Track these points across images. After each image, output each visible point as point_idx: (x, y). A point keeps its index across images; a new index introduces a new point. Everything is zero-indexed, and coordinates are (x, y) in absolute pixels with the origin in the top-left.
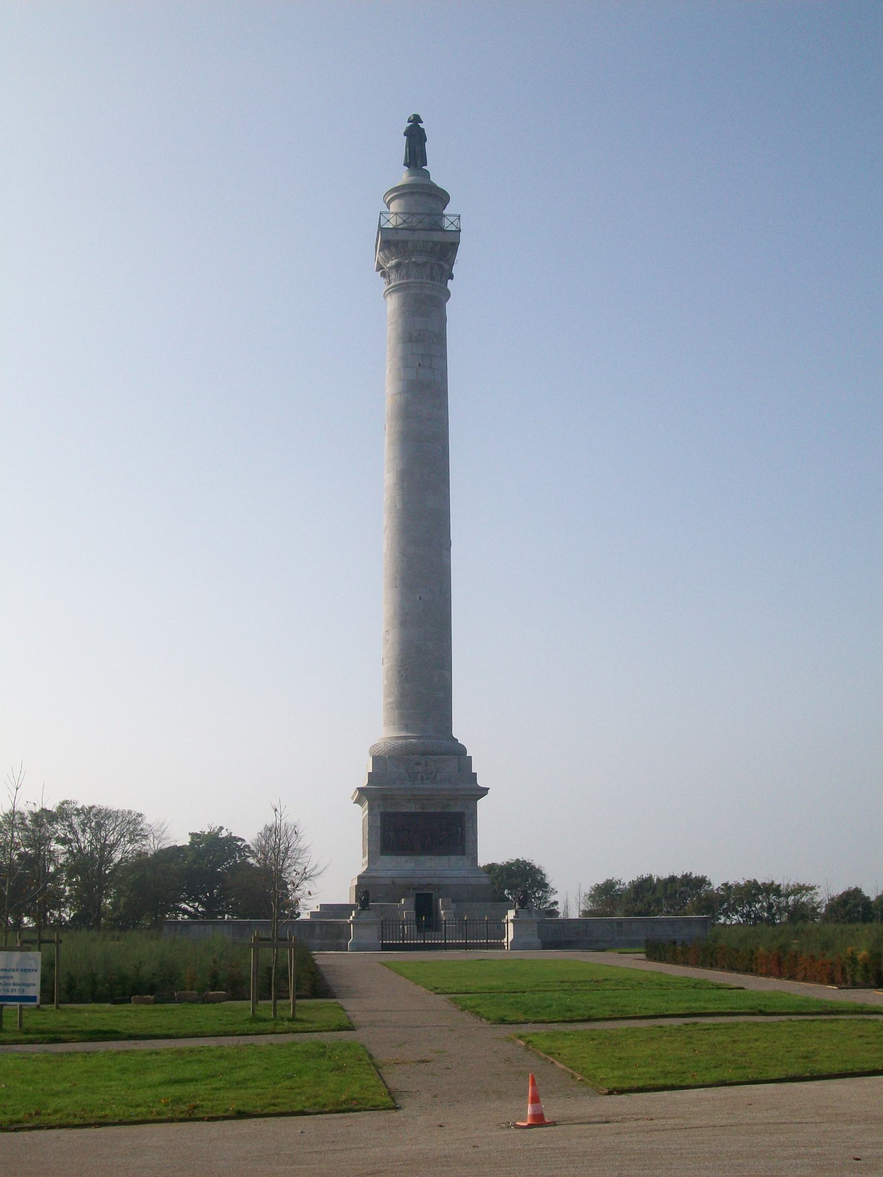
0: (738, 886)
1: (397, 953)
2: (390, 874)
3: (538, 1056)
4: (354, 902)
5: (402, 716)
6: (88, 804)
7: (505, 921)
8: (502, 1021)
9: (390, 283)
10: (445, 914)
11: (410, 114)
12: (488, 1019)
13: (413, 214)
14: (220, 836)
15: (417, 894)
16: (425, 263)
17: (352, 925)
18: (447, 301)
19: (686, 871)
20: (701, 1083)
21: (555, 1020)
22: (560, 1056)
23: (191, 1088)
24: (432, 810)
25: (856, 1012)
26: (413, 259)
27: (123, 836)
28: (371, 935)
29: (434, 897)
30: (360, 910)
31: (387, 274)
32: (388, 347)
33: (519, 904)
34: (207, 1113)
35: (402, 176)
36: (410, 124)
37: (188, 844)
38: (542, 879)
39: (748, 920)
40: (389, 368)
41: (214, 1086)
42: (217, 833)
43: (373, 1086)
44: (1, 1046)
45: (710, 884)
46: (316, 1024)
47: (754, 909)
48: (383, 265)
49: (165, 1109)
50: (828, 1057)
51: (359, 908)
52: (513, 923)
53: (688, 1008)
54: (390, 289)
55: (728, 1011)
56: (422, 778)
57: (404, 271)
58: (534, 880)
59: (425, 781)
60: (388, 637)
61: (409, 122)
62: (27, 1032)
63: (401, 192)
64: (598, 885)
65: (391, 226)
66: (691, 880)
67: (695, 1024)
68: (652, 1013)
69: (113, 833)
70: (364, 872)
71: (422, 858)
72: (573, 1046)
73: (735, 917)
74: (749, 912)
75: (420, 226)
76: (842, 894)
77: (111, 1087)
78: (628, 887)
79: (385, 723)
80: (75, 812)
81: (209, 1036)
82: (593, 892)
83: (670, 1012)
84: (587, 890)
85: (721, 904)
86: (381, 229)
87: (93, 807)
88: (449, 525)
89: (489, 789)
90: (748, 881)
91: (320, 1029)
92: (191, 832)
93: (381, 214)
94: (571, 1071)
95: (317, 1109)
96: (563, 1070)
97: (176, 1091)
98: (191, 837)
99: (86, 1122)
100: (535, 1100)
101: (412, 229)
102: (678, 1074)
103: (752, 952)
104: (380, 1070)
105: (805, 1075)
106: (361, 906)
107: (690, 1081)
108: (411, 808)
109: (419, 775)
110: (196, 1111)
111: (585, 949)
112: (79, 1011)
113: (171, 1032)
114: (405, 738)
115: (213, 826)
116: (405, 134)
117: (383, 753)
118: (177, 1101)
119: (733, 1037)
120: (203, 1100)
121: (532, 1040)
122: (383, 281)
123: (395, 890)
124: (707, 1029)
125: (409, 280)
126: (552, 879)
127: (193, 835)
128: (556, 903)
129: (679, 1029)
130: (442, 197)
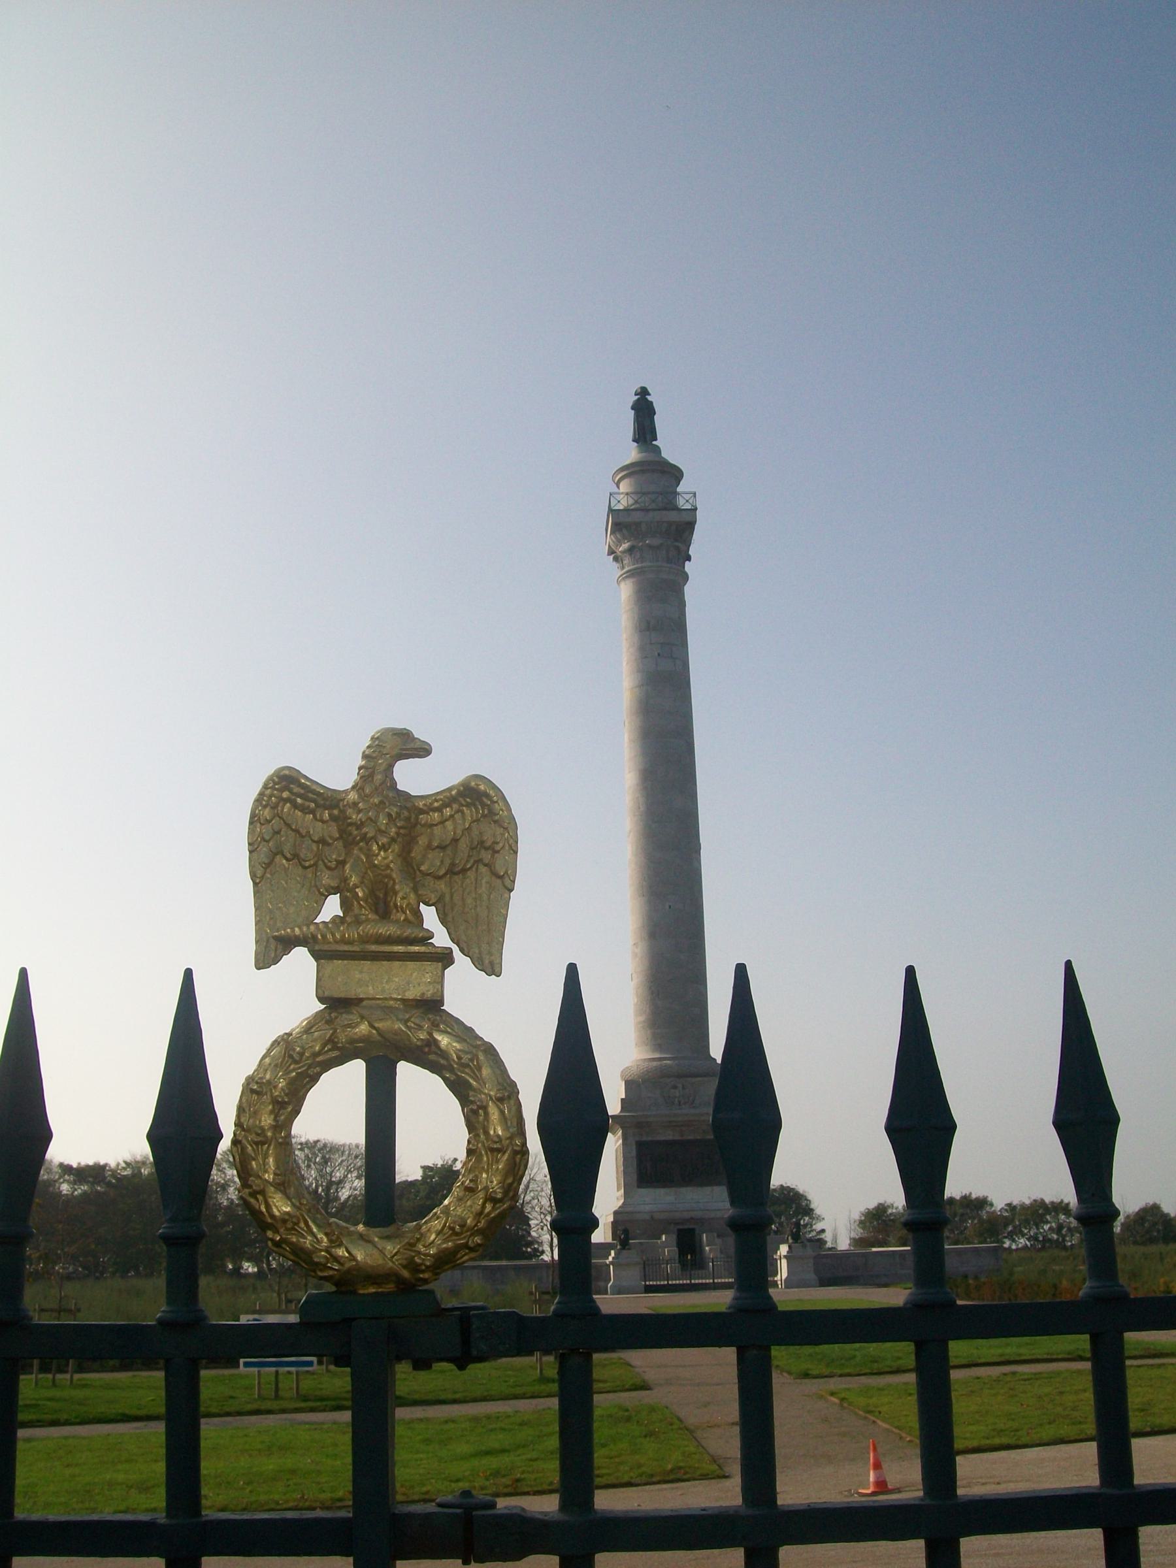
0: (1023, 1207)
1: (663, 1296)
2: (648, 1208)
3: (856, 1414)
4: (609, 1240)
5: (655, 1036)
6: (312, 1138)
7: (777, 1257)
8: (806, 1375)
9: (623, 568)
10: (710, 1250)
11: (636, 387)
12: (789, 1373)
13: (644, 494)
14: (454, 1169)
15: (679, 1231)
17: (611, 1267)
18: (685, 584)
19: (966, 1192)
20: (1038, 1442)
21: (863, 1372)
22: (881, 1415)
23: (506, 1459)
24: (691, 1137)
26: (647, 542)
27: (350, 1172)
28: (633, 1276)
29: (697, 1232)
30: (621, 1249)
31: (619, 558)
32: (624, 636)
33: (792, 1238)
34: (531, 1486)
35: (631, 453)
36: (637, 397)
37: (420, 1178)
38: (807, 1205)
39: (1036, 1243)
40: (625, 659)
41: (529, 1456)
42: (451, 1166)
43: (695, 1454)
45: (992, 1205)
46: (608, 1384)
47: (1042, 1231)
48: (614, 549)
49: (487, 1483)
50: (1164, 1409)
51: (619, 1247)
52: (787, 1259)
53: (1001, 1355)
54: (624, 574)
55: (1045, 1356)
56: (680, 1102)
57: (638, 555)
58: (799, 1206)
59: (683, 1106)
60: (636, 950)
61: (636, 395)
62: (306, 1399)
63: (631, 471)
64: (868, 1209)
65: (622, 508)
66: (971, 1201)
67: (1014, 1373)
68: (964, 1362)
69: (339, 1169)
70: (620, 1207)
71: (683, 1190)
72: (891, 1403)
73: (1022, 1241)
74: (1036, 1234)
75: (653, 506)
76: (1139, 1211)
77: (421, 1460)
78: (902, 1211)
79: (636, 1045)
80: (299, 1147)
81: (498, 1400)
82: (863, 1218)
83: (983, 1360)
84: (856, 1216)
85: (1006, 1225)
86: (611, 510)
87: (318, 1141)
90: (1035, 1201)
91: (615, 1389)
92: (423, 1165)
93: (611, 494)
94: (897, 1431)
95: (644, 1479)
96: (887, 1429)
97: (493, 1462)
98: (423, 1171)
99: (409, 1499)
100: (877, 1466)
101: (645, 510)
102: (1012, 1431)
103: (1055, 1286)
104: (695, 1435)
105: (1145, 1430)
106: (620, 1245)
107: (1024, 1440)
108: (669, 1135)
109: (676, 1100)
110: (519, 1484)
111: (866, 1284)
113: (457, 1396)
114: (660, 1059)
115: (447, 1158)
116: (632, 409)
117: (636, 1077)
118: (496, 1473)
119: (1058, 1388)
120: (523, 1472)
121: (847, 1397)
122: (616, 565)
123: (655, 1227)
124: (1028, 1379)
125: (644, 564)
126: (819, 1204)
127: (425, 1168)
128: (823, 1231)
129: (998, 1380)
130: (674, 474)
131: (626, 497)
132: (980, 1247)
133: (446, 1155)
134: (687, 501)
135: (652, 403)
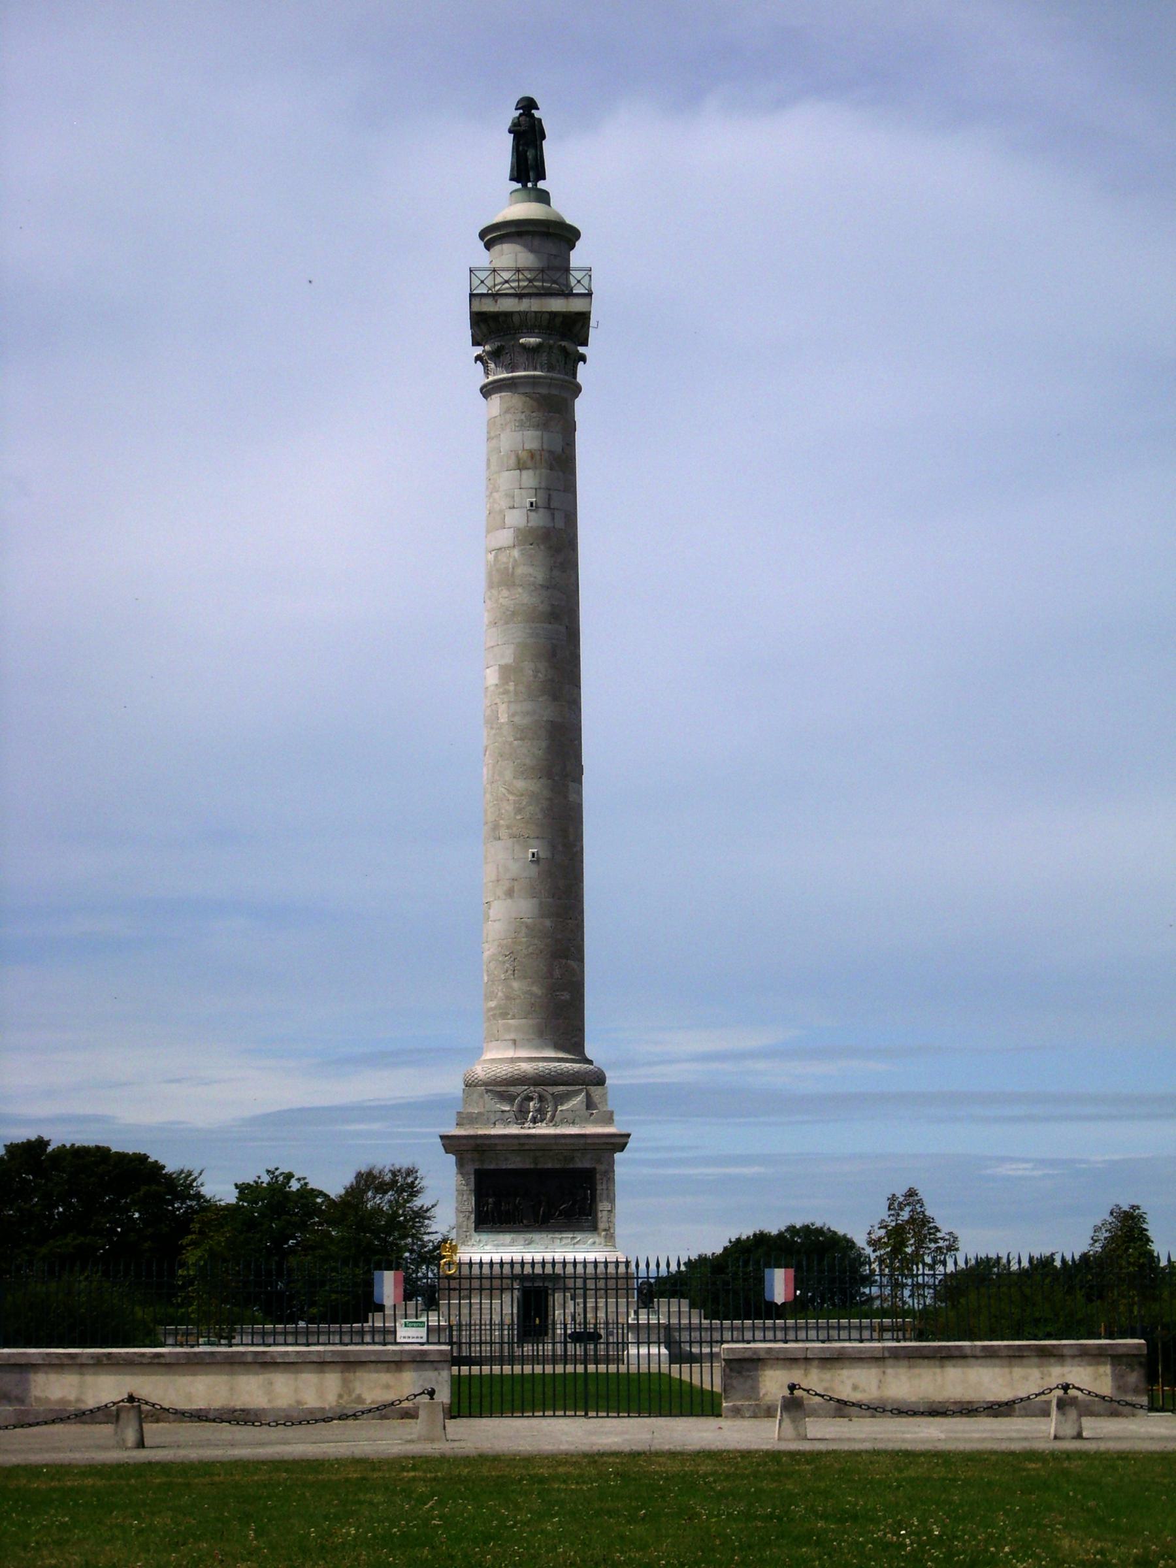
16: (539, 345)
24: (550, 1166)
25: (861, 1358)
88: (516, 1141)
89: (628, 1136)
93: (471, 271)
116: (510, 132)
131: (492, 276)
132: (939, 1340)
133: (277, 1169)
135: (540, 120)
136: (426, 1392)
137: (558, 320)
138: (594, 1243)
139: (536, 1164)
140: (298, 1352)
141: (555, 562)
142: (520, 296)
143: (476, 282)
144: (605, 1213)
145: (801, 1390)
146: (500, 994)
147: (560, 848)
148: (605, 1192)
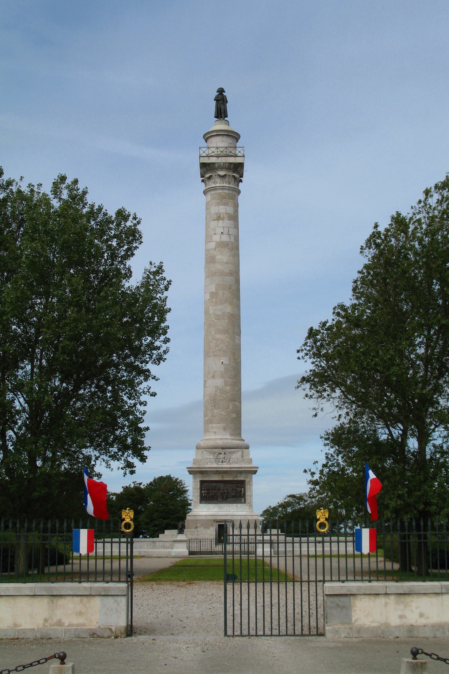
16: (225, 175)
25: (428, 594)
44: (0, 604)
56: (222, 461)
112: (181, 538)
116: (215, 100)
134: (240, 152)
136: (57, 656)
137: (232, 166)
138: (245, 508)
139: (223, 478)
140: (15, 588)
141: (231, 254)
142: (218, 157)
143: (202, 152)
144: (249, 497)
145: (423, 654)
146: (210, 415)
147: (232, 360)
148: (249, 489)
